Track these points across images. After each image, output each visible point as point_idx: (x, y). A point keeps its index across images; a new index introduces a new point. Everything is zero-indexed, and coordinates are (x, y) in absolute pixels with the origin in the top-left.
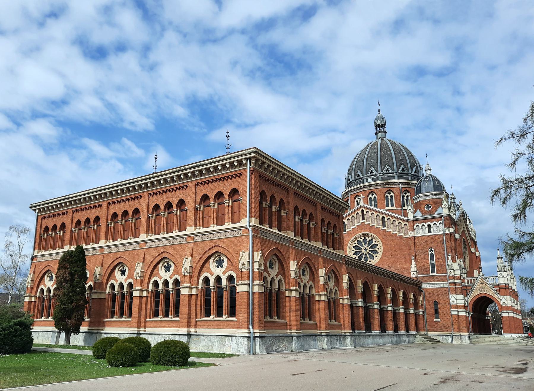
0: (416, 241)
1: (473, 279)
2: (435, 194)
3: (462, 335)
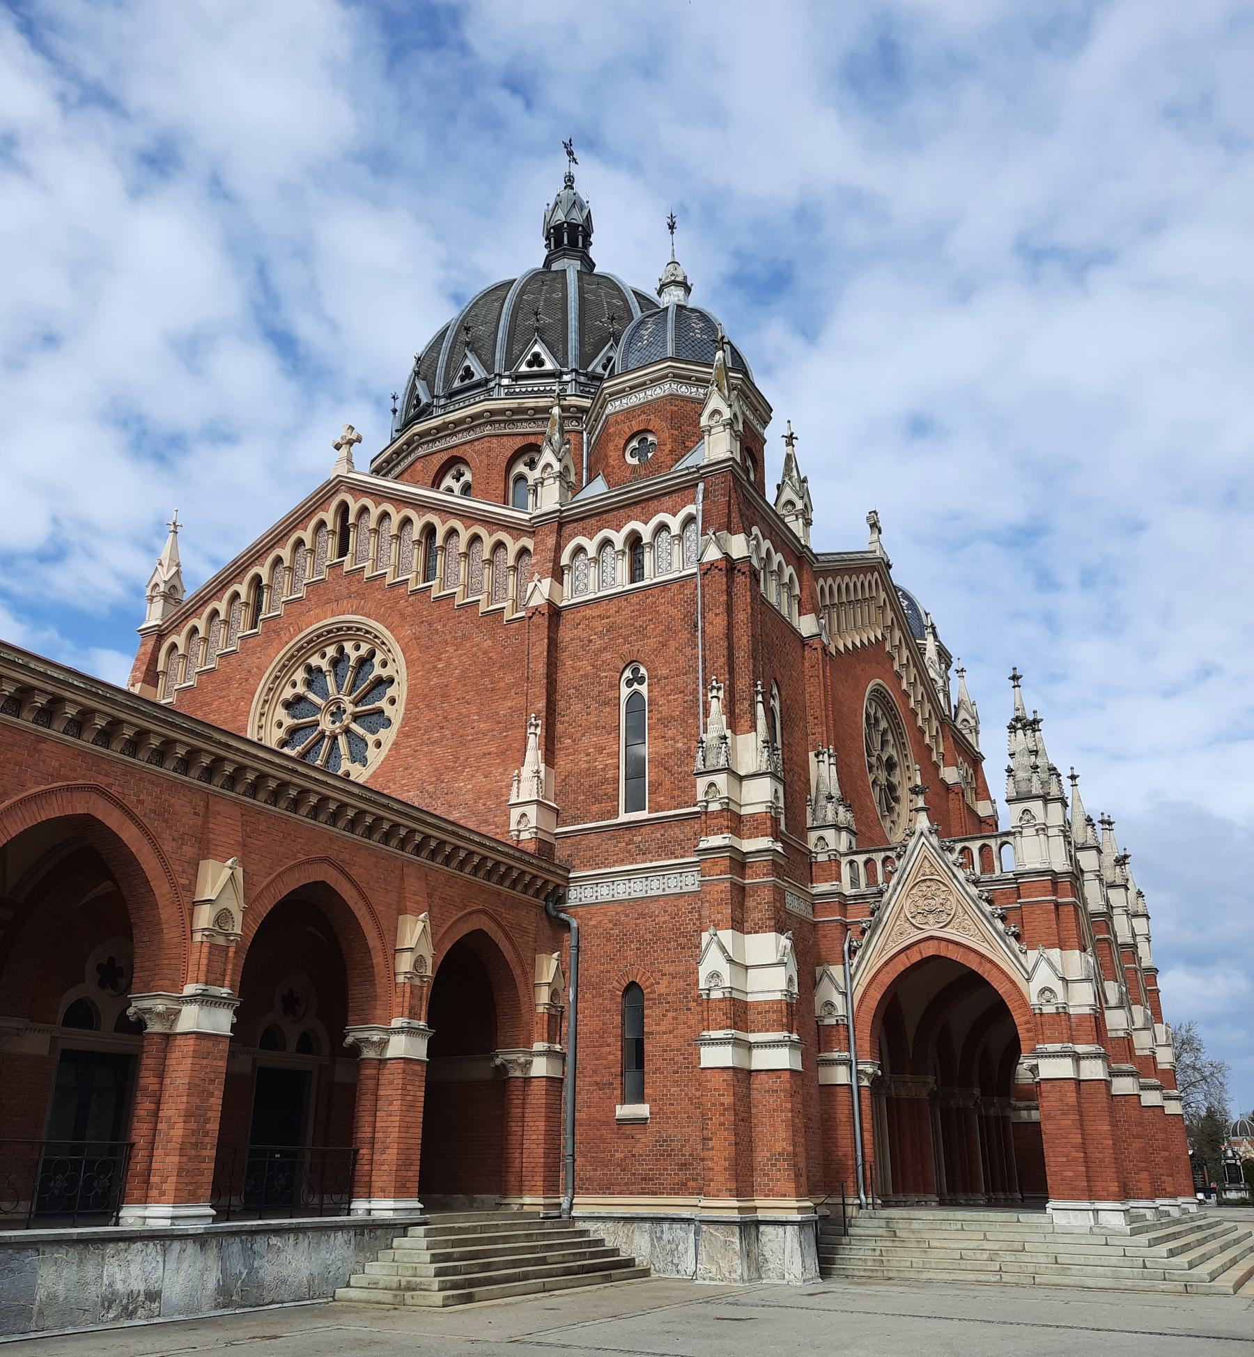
0: (566, 634)
1: (878, 857)
2: (675, 376)
3: (760, 1215)
